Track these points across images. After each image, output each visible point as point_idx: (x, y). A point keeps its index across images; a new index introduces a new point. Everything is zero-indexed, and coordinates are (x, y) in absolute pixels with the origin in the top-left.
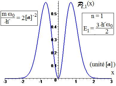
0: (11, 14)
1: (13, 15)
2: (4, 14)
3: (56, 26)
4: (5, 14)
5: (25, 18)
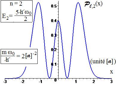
0: (11, 52)
1: (13, 54)
2: (4, 52)
3: (56, 19)
4: (5, 52)
5: (25, 57)
